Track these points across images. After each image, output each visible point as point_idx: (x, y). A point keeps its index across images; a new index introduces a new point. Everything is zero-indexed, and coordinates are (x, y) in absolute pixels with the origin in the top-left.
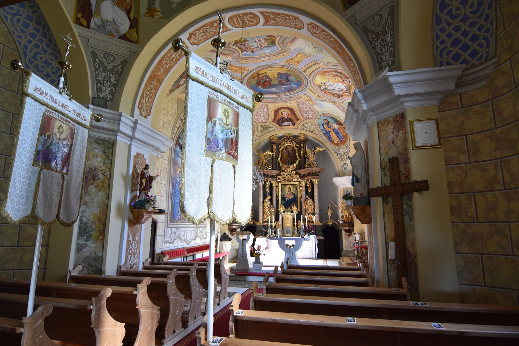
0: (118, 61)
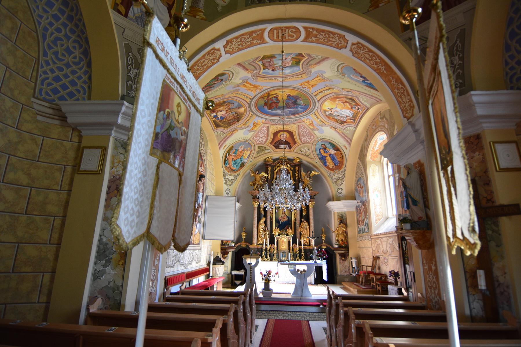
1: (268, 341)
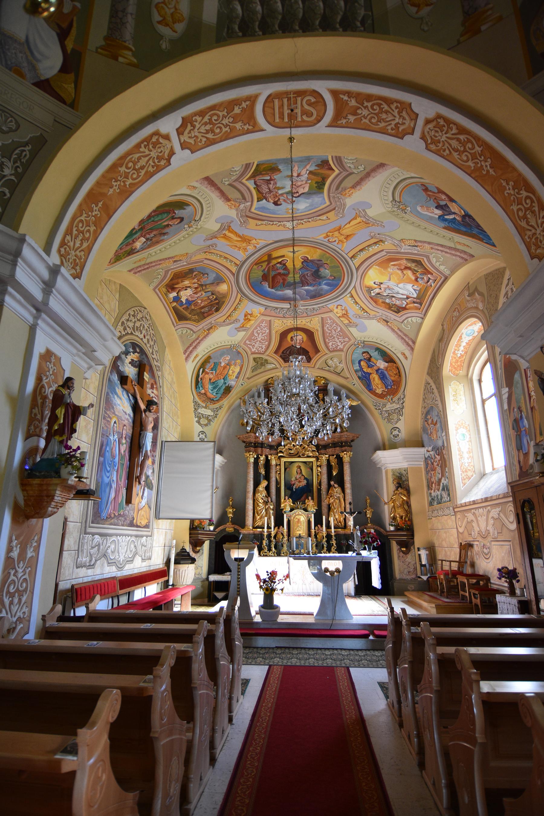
0: (26, 134)
1: (267, 716)
